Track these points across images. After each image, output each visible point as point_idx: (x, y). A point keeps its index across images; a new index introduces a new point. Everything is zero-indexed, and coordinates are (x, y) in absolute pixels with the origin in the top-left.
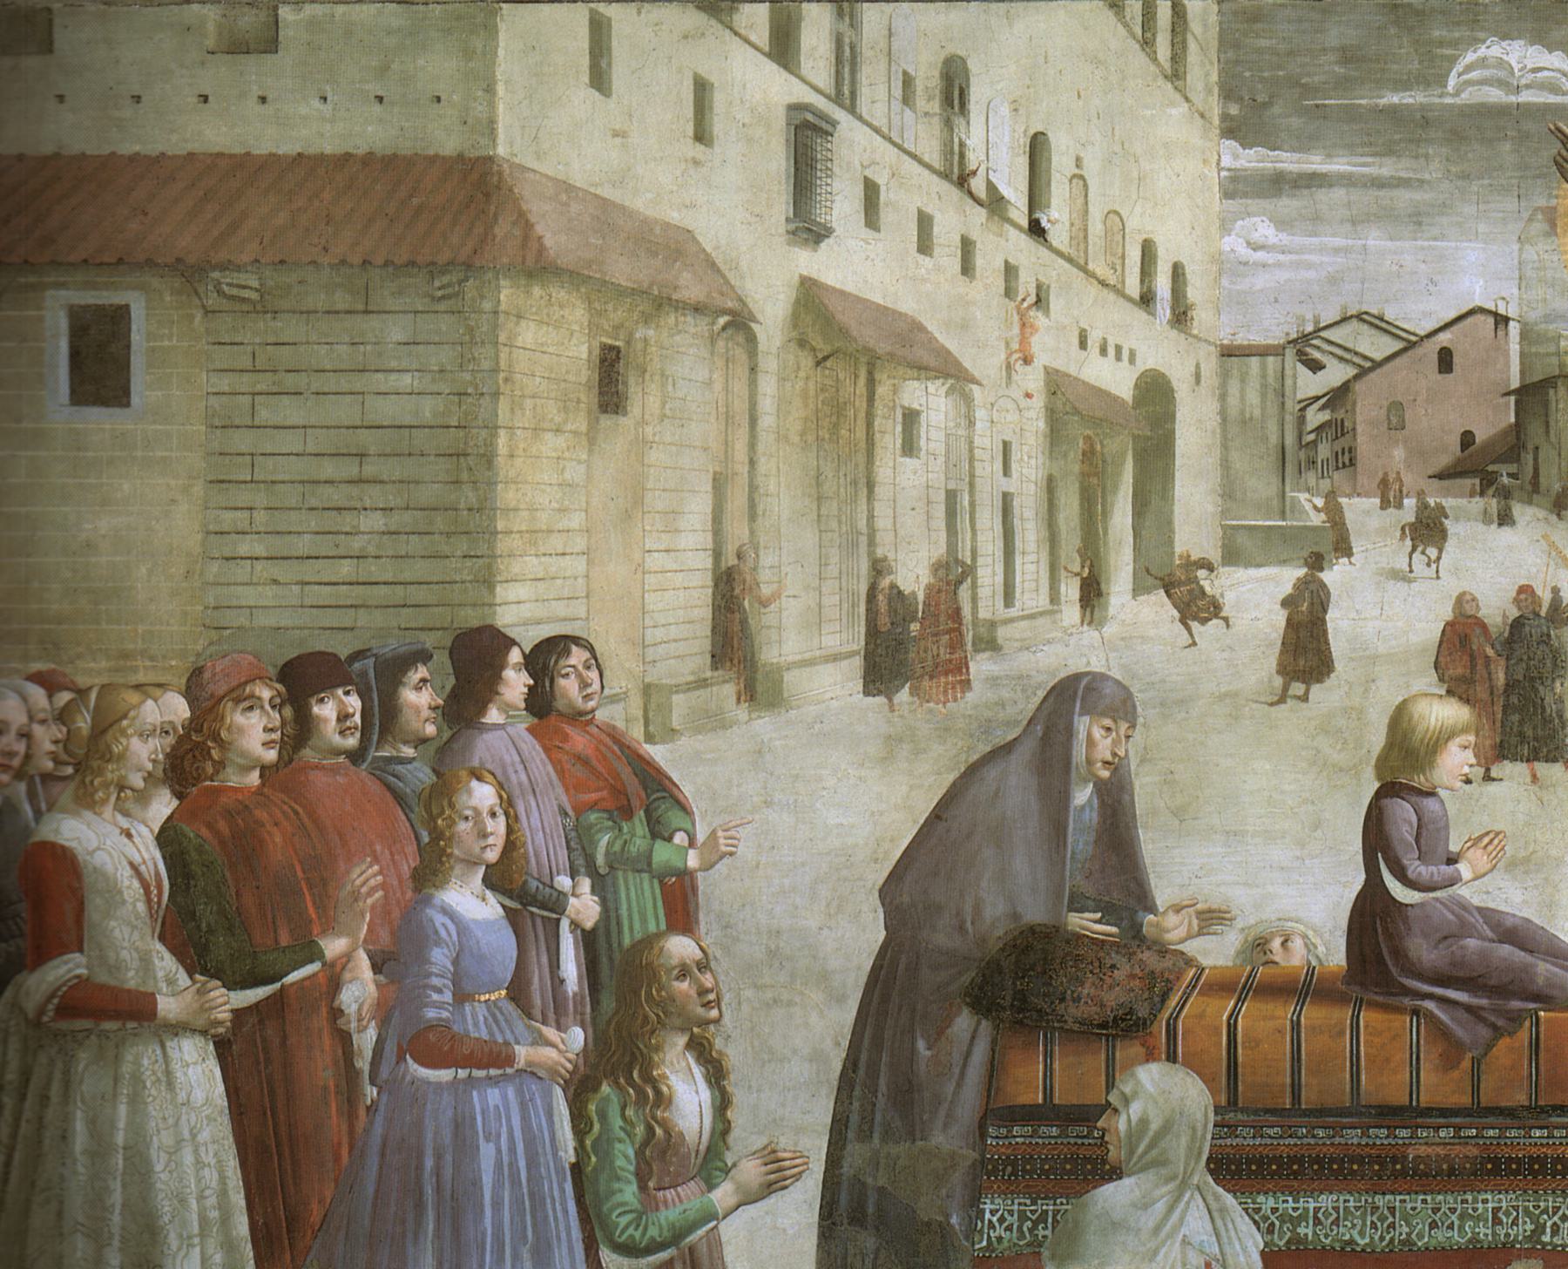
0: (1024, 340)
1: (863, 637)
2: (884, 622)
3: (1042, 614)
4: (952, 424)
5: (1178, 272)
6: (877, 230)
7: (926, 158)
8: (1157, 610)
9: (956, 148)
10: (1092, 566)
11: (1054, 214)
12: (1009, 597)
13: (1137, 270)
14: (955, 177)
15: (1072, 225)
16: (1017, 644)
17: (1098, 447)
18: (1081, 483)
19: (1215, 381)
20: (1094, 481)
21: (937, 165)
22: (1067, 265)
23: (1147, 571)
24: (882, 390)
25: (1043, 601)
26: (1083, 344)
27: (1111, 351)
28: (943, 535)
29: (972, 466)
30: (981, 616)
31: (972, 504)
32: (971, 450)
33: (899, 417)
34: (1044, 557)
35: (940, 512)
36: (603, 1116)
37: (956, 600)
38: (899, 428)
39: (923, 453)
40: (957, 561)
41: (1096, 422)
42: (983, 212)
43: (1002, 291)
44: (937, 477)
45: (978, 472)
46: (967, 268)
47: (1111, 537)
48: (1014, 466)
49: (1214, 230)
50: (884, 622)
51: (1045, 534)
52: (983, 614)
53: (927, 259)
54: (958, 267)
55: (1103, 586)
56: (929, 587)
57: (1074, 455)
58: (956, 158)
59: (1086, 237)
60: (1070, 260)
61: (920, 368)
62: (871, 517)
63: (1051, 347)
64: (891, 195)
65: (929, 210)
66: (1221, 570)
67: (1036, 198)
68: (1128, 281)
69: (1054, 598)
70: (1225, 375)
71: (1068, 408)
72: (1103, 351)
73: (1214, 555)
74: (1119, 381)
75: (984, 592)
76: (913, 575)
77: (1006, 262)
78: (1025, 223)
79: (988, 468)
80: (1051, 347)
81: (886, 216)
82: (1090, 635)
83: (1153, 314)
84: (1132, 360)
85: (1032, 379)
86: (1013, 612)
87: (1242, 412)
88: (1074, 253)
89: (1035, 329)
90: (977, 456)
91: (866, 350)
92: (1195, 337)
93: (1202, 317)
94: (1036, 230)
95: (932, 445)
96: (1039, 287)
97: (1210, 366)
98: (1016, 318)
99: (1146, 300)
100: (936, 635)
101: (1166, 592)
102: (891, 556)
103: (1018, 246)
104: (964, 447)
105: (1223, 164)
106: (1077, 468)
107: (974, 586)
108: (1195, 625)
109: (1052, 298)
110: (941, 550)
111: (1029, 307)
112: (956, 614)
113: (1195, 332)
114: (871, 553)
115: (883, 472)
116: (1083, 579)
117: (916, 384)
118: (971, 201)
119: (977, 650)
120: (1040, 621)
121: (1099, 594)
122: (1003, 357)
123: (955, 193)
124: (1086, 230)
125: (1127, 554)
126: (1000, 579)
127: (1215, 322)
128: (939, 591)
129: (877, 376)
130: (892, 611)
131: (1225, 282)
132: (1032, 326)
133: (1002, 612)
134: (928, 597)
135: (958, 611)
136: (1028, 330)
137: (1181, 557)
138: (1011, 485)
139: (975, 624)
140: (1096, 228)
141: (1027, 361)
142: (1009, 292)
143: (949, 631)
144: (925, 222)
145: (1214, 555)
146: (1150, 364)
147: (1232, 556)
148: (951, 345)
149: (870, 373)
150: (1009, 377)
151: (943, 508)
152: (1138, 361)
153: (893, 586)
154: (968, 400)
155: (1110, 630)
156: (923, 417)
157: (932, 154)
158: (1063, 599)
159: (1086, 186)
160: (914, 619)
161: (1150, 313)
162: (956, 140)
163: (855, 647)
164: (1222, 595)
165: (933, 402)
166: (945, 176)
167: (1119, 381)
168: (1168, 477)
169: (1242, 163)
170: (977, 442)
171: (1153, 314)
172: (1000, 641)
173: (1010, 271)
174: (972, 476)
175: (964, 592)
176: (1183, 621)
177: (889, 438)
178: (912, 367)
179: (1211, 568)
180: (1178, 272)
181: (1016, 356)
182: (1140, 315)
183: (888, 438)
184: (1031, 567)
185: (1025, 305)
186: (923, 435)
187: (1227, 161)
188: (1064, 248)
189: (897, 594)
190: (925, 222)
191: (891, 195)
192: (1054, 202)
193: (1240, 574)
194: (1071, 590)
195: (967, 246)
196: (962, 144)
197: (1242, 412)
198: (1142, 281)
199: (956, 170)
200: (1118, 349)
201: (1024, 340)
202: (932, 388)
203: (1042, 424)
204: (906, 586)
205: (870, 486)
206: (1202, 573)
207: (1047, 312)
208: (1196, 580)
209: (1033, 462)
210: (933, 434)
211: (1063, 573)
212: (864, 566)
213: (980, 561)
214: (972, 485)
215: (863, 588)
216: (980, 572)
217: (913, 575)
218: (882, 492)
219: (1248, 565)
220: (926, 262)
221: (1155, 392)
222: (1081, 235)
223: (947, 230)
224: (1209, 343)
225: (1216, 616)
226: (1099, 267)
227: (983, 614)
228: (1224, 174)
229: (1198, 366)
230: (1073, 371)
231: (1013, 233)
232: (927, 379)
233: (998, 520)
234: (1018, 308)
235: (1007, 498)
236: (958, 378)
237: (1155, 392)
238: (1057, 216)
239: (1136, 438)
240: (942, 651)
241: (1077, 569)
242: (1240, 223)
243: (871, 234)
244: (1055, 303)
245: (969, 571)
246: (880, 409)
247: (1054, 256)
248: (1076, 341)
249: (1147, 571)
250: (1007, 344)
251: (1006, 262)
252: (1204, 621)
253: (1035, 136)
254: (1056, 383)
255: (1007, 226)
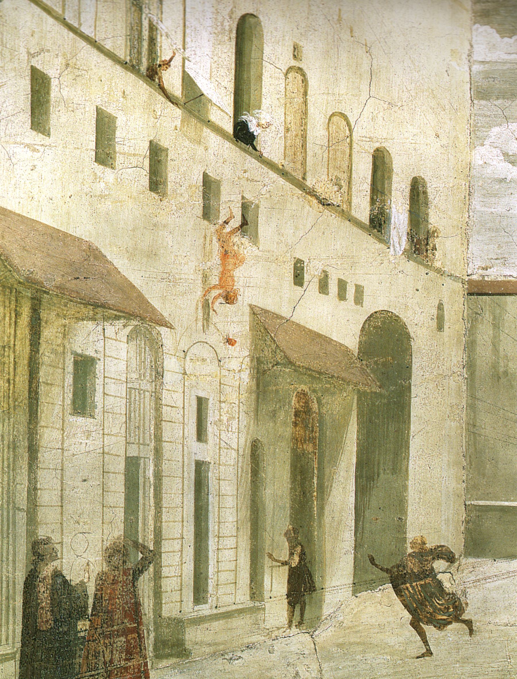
0: (225, 275)
1: (19, 638)
2: (45, 618)
3: (240, 611)
4: (134, 376)
5: (417, 192)
6: (47, 133)
7: (108, 45)
8: (384, 611)
9: (146, 34)
10: (302, 555)
11: (265, 116)
12: (200, 592)
13: (367, 187)
14: (143, 68)
15: (287, 130)
16: (207, 650)
17: (315, 406)
18: (294, 451)
19: (460, 327)
20: (309, 447)
21: (122, 53)
22: (281, 181)
23: (372, 560)
24: (49, 333)
25: (242, 597)
26: (298, 278)
27: (333, 288)
28: (121, 514)
29: (158, 427)
30: (165, 613)
31: (158, 476)
32: (158, 408)
33: (70, 368)
34: (245, 544)
35: (118, 485)
36: (144, 641)
37: (135, 595)
38: (69, 379)
39: (98, 411)
40: (136, 544)
41: (315, 375)
42: (178, 112)
43: (200, 212)
44: (116, 444)
45: (166, 436)
46: (156, 183)
47: (327, 519)
48: (211, 429)
49: (464, 139)
50: (45, 618)
51: (245, 513)
52: (169, 610)
53: (108, 170)
54: (145, 181)
55: (317, 579)
56: (102, 578)
57: (285, 415)
58: (145, 44)
59: (304, 146)
60: (283, 173)
61: (96, 306)
62: (33, 490)
63: (260, 282)
64: (65, 93)
65: (110, 110)
66: (463, 561)
67: (243, 96)
68: (355, 201)
69: (256, 590)
70: (473, 319)
71: (278, 359)
72: (323, 287)
73: (455, 542)
74: (340, 325)
75: (169, 584)
76: (82, 562)
77: (205, 176)
78: (229, 128)
79: (179, 428)
80: (260, 282)
81: (58, 117)
82: (299, 640)
83: (385, 241)
84: (359, 300)
85: (234, 321)
86: (205, 610)
87: (495, 366)
88: (289, 167)
89: (240, 261)
90: (165, 417)
91: (30, 282)
92: (439, 271)
93: (447, 249)
94: (243, 135)
95: (110, 400)
96: (245, 207)
97: (456, 306)
98: (216, 245)
99: (378, 223)
100: (109, 636)
101: (394, 587)
102: (56, 538)
103: (220, 154)
104: (148, 403)
105: (476, 57)
106: (288, 431)
107: (158, 576)
108: (430, 630)
109: (262, 219)
110: (117, 531)
111: (233, 232)
112: (135, 611)
113: (438, 264)
114: (31, 533)
115: (49, 436)
116: (291, 569)
117: (90, 325)
118: (161, 98)
119: (159, 657)
120: (237, 622)
121: (312, 588)
122: (200, 293)
123: (140, 89)
124: (304, 137)
125: (347, 538)
126: (189, 568)
127: (457, 254)
128: (114, 582)
129: (44, 315)
130: (55, 603)
131: (476, 203)
132: (235, 256)
133: (190, 609)
134: (100, 588)
135: (137, 606)
136: (231, 261)
137: (413, 543)
138: (206, 452)
139: (157, 626)
140: (317, 132)
141: (229, 298)
142: (207, 213)
143: (126, 632)
144: (104, 127)
145: (455, 542)
146: (381, 305)
147: (478, 544)
148: (135, 278)
149: (35, 311)
150: (207, 318)
151: (121, 479)
152: (367, 299)
153: (57, 574)
154: (156, 346)
155: (325, 634)
156: (99, 366)
157: (120, 48)
158: (266, 595)
159: (305, 81)
160: (82, 613)
161: (381, 241)
162: (146, 24)
163: (9, 650)
164: (464, 593)
165: (113, 349)
166: (131, 67)
167: (340, 325)
168: (401, 444)
169: (499, 55)
170: (166, 398)
171: (385, 241)
172: (188, 645)
173: (209, 186)
174: (158, 438)
175: (145, 584)
176: (415, 624)
177: (57, 395)
178: (86, 305)
179: (451, 558)
180: (417, 192)
181: (215, 293)
182: (370, 243)
183: (56, 390)
184: (228, 554)
185: (228, 229)
186: (99, 389)
187: (481, 52)
188: (277, 158)
189: (61, 584)
190: (104, 127)
191: (65, 93)
192: (265, 102)
193: (489, 567)
194: (276, 584)
195: (156, 154)
196: (152, 28)
197: (495, 366)
198: (373, 201)
199: (144, 61)
200: (342, 285)
201: (225, 275)
202: (110, 330)
203: (246, 377)
204: (74, 577)
205: (33, 451)
206: (440, 565)
207: (255, 239)
208: (432, 573)
209: (235, 424)
210: (112, 388)
211: (267, 562)
212: (22, 549)
213: (166, 546)
214: (158, 452)
215: (21, 576)
216: (165, 559)
217: (82, 562)
218: (47, 457)
219: (497, 556)
220: (108, 175)
221: (386, 343)
222: (299, 142)
223: (133, 135)
224: (456, 278)
225: (457, 619)
226: (318, 180)
227: (169, 610)
228: (476, 68)
229: (440, 307)
230: (285, 312)
231: (214, 140)
232: (105, 319)
233: (190, 496)
234: (219, 232)
235: (200, 467)
236: (143, 319)
237: (386, 343)
238: (269, 118)
239: (361, 395)
240: (116, 656)
241: (284, 556)
242: (496, 130)
243: (38, 138)
244: (265, 229)
245: (152, 557)
246: (46, 355)
247: (266, 169)
248: (290, 276)
249: (372, 560)
250: (205, 278)
251: (205, 176)
252: (441, 625)
253: (244, 18)
254: (264, 324)
255: (206, 131)
